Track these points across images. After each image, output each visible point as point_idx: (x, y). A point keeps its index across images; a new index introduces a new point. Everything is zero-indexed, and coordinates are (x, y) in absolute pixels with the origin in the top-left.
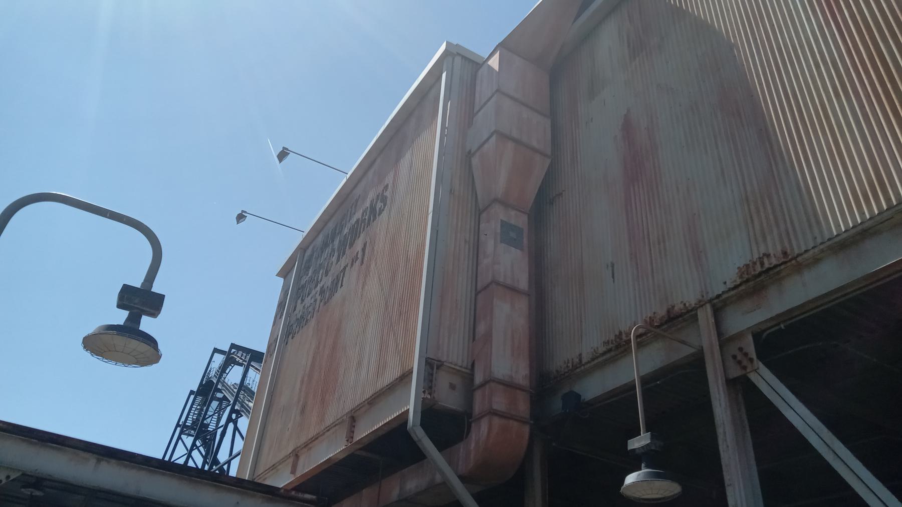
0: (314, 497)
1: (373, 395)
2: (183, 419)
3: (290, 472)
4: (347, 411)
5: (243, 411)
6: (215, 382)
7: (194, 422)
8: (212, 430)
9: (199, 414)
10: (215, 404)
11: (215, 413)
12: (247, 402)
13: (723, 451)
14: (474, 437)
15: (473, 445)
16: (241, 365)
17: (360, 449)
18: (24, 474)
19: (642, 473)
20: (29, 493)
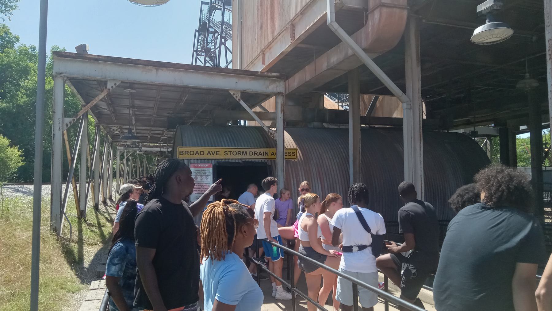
0: (278, 74)
1: (303, 8)
2: (196, 47)
3: (262, 64)
4: (288, 21)
5: (227, 37)
6: (207, 22)
7: (202, 48)
8: (213, 51)
9: (204, 43)
10: (211, 36)
11: (212, 41)
12: (229, 31)
13: (547, 3)
14: (370, 24)
15: (370, 28)
16: (219, 9)
17: (300, 43)
18: (122, 82)
19: (486, 25)
20: (129, 92)
